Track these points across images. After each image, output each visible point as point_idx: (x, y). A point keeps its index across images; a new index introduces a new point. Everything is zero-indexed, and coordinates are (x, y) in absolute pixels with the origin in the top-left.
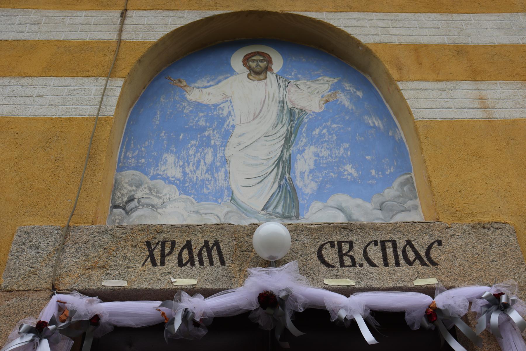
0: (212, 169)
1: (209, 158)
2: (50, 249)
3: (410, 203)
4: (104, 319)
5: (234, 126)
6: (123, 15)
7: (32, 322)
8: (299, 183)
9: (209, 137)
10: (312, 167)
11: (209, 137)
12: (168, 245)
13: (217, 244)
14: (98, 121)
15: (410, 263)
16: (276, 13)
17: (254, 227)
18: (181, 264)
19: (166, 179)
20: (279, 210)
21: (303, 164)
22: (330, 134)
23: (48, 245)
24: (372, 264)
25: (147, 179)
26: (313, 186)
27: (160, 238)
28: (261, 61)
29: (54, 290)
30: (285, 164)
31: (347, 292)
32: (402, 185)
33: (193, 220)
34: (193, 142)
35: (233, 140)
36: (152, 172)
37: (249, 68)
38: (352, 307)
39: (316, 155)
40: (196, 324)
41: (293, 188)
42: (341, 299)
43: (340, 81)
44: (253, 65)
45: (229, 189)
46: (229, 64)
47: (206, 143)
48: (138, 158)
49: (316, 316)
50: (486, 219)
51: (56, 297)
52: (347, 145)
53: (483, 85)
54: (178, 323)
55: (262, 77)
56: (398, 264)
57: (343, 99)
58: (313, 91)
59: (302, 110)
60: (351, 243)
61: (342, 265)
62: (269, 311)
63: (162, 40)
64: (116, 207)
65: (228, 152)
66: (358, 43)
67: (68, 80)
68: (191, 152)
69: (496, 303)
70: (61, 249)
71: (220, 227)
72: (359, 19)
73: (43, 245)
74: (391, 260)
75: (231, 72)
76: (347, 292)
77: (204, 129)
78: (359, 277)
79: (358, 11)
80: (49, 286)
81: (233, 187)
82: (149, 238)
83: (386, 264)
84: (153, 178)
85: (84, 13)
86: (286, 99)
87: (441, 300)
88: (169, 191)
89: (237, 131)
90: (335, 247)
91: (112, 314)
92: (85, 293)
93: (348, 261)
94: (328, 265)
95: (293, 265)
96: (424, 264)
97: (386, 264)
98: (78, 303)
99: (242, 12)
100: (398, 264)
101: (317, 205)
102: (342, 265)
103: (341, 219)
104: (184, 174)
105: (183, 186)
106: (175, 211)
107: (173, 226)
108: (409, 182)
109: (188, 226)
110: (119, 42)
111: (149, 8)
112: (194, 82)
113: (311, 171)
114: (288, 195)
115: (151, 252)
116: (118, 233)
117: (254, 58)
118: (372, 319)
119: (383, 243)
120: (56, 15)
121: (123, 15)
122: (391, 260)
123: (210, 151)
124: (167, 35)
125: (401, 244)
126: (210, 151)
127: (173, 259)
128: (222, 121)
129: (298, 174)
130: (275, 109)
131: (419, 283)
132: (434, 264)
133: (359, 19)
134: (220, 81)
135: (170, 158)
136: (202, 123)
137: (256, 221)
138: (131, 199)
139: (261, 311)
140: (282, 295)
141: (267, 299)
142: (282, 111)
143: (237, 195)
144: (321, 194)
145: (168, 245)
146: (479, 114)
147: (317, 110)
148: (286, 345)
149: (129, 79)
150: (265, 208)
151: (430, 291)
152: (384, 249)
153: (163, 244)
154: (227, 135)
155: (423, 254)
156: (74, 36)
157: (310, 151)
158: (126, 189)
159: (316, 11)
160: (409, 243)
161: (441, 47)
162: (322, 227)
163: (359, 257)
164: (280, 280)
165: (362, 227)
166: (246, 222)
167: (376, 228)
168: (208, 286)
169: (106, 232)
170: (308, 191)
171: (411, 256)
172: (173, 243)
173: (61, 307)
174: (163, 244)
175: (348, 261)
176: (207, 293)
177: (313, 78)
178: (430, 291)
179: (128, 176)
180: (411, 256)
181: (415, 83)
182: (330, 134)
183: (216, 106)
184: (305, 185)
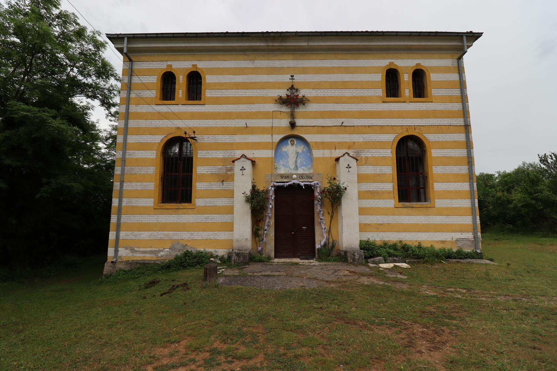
21: (298, 162)
30: (296, 162)
38: (302, 184)
47: (285, 158)
49: (299, 184)
57: (305, 150)
58: (301, 148)
69: (317, 184)
88: (281, 166)
90: (301, 176)
98: (275, 184)
105: (283, 165)
106: (282, 171)
114: (296, 168)
120: (262, 136)
146: (322, 156)
156: (266, 141)
179: (276, 164)
184: (299, 165)
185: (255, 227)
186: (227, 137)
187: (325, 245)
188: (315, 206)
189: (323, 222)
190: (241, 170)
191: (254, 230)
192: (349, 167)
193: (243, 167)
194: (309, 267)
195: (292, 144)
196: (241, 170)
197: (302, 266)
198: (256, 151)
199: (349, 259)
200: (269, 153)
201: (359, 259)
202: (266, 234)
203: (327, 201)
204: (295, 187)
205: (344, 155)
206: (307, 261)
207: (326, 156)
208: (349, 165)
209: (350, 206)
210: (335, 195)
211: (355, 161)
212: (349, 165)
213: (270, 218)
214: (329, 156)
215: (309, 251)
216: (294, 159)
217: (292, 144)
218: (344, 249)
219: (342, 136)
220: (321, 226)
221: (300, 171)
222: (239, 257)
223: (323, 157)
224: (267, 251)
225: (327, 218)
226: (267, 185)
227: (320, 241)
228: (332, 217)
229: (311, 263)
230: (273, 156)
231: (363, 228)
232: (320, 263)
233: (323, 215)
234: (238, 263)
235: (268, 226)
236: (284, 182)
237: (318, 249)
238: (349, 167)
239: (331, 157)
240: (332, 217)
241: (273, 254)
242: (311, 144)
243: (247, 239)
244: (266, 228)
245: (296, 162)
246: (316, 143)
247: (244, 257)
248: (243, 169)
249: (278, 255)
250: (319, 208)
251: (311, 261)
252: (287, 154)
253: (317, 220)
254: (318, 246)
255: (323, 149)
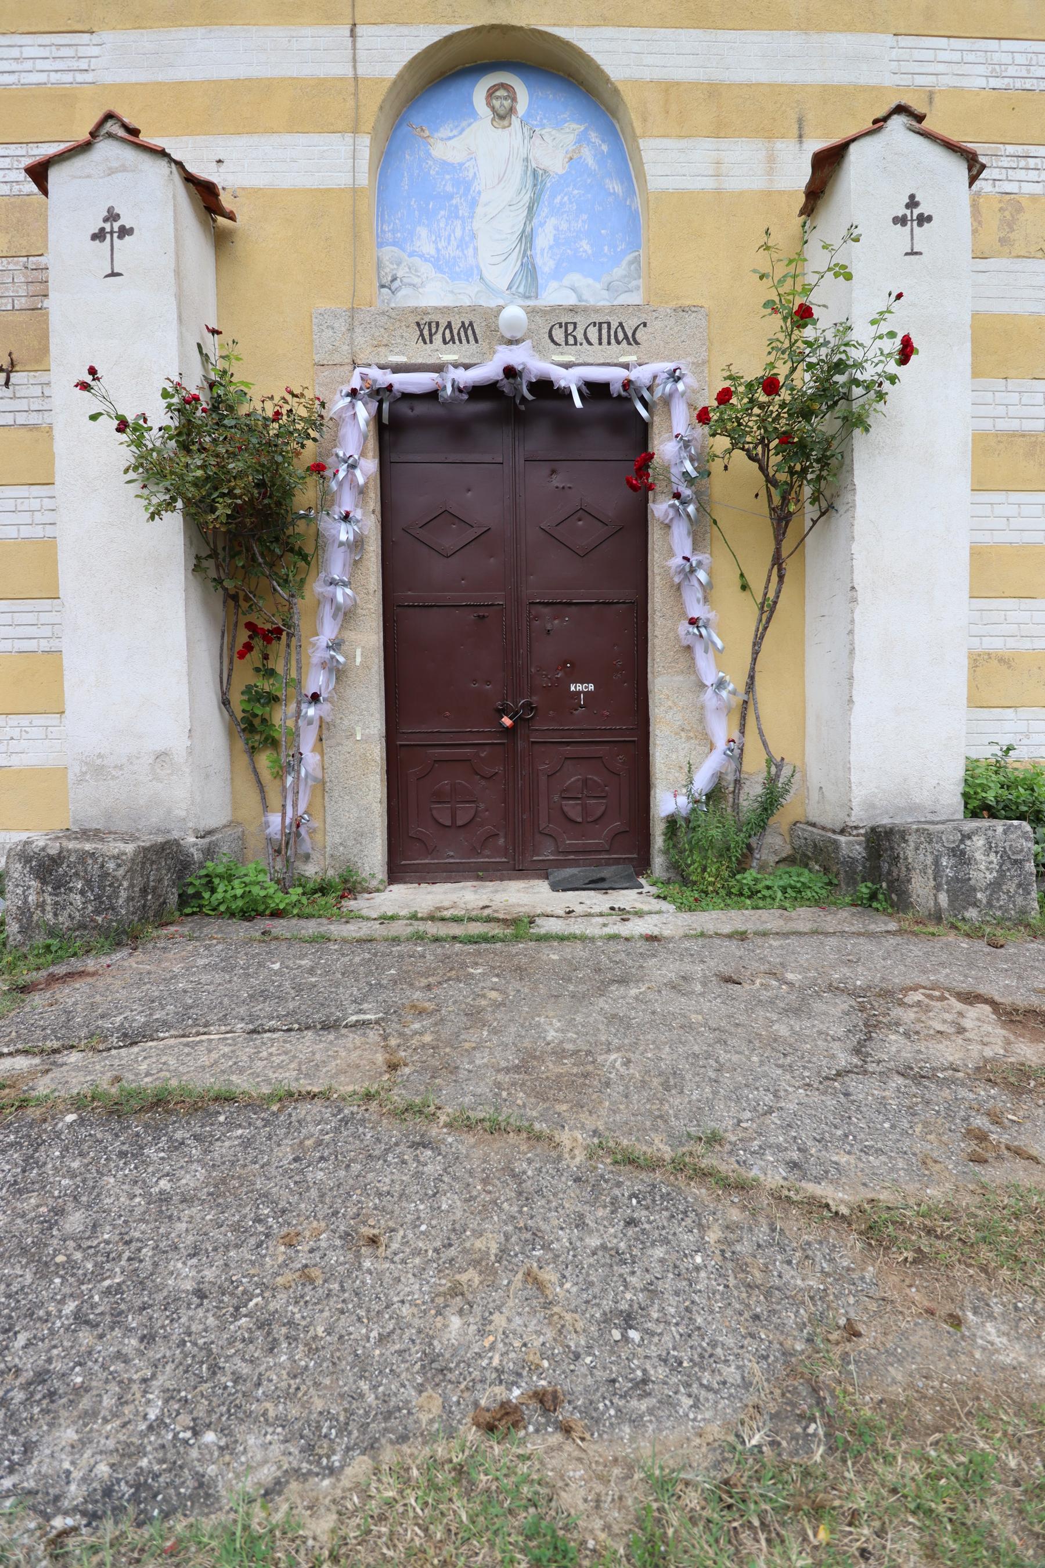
0: (462, 245)
1: (458, 233)
2: (343, 329)
3: (634, 283)
4: (396, 387)
5: (479, 193)
6: (353, 34)
7: (347, 389)
8: (539, 261)
9: (456, 207)
10: (552, 242)
11: (456, 207)
12: (434, 325)
13: (471, 324)
14: (355, 191)
15: (619, 343)
16: (521, 28)
17: (501, 308)
18: (445, 342)
19: (422, 256)
20: (521, 290)
21: (543, 240)
22: (571, 203)
23: (341, 325)
24: (590, 343)
25: (405, 256)
26: (551, 264)
27: (427, 319)
28: (505, 98)
29: (355, 364)
30: (527, 238)
31: (567, 366)
32: (630, 263)
33: (448, 301)
34: (442, 213)
35: (479, 210)
36: (409, 249)
37: (493, 109)
38: (569, 379)
39: (556, 228)
40: (460, 391)
41: (534, 266)
42: (562, 371)
43: (586, 129)
44: (496, 103)
45: (478, 267)
46: (472, 103)
47: (454, 214)
48: (394, 231)
49: (544, 387)
50: (688, 302)
51: (358, 370)
52: (585, 217)
53: (724, 143)
54: (449, 390)
55: (506, 123)
56: (609, 343)
57: (588, 155)
59: (545, 171)
60: (575, 324)
61: (567, 343)
62: (511, 380)
63: (400, 76)
64: (383, 286)
65: (477, 224)
66: (607, 80)
67: (316, 138)
68: (442, 225)
69: (674, 376)
70: (351, 330)
71: (473, 309)
72: (612, 39)
73: (336, 325)
74: (605, 340)
75: (473, 114)
76: (567, 366)
77: (451, 197)
78: (578, 354)
79: (613, 25)
80: (350, 361)
81: (482, 265)
82: (418, 319)
83: (600, 343)
84: (410, 255)
85: (308, 31)
86: (531, 157)
87: (634, 375)
88: (426, 269)
89: (483, 198)
90: (563, 328)
91: (401, 383)
92: (382, 367)
93: (571, 340)
94: (556, 344)
95: (528, 343)
96: (629, 344)
97: (600, 343)
98: (374, 373)
99: (483, 27)
100: (609, 343)
101: (554, 284)
102: (567, 343)
103: (571, 300)
104: (438, 250)
105: (438, 263)
106: (433, 293)
107: (436, 308)
108: (637, 260)
109: (448, 308)
110: (356, 78)
111: (379, 20)
112: (437, 130)
113: (551, 247)
115: (421, 331)
116: (393, 315)
117: (498, 93)
118: (584, 389)
119: (600, 324)
121: (353, 34)
122: (605, 340)
123: (459, 223)
124: (405, 66)
125: (614, 325)
126: (459, 223)
127: (438, 338)
128: (468, 185)
129: (538, 251)
130: (518, 168)
131: (623, 359)
132: (637, 343)
133: (612, 39)
134: (463, 130)
135: (423, 231)
136: (449, 188)
137: (501, 302)
138: (394, 279)
139: (505, 381)
140: (520, 368)
141: (510, 372)
142: (526, 173)
143: (485, 274)
144: (557, 274)
145: (434, 325)
146: (709, 184)
147: (561, 172)
148: (523, 408)
149: (374, 133)
150: (509, 288)
151: (626, 366)
152: (600, 330)
153: (430, 324)
154: (474, 204)
155: (630, 335)
156: (308, 71)
157: (552, 221)
158: (389, 269)
159: (567, 25)
160: (621, 324)
161: (695, 85)
162: (554, 309)
163: (580, 337)
164: (518, 356)
165: (585, 310)
166: (493, 303)
167: (597, 310)
168: (467, 361)
169: (383, 313)
170: (546, 269)
171: (621, 336)
172: (437, 324)
173: (364, 377)
174: (430, 324)
175: (571, 340)
176: (467, 367)
177: (558, 126)
178: (626, 366)
179: (388, 252)
180: (621, 336)
181: (658, 140)
182: (571, 203)
183: (461, 165)
184: (545, 263)
185: (245, 675)
186: (32, 47)
187: (715, 795)
188: (655, 535)
189: (709, 645)
190: (99, 236)
191: (237, 700)
192: (913, 215)
193: (112, 216)
194: (610, 968)
195: (502, 116)
196: (99, 236)
197: (553, 955)
198: (242, 141)
199: (920, 888)
200: (332, 161)
201: (996, 886)
202: (323, 725)
203: (738, 479)
204: (516, 405)
205: (880, 122)
206: (595, 901)
207: (733, 184)
208: (912, 203)
209: (911, 500)
210: (804, 441)
211: (959, 170)
212: (912, 203)
213: (347, 615)
214: (758, 183)
215: (609, 829)
216: (514, 222)
217: (502, 116)
218: (860, 817)
219: (844, 42)
220: (692, 667)
221: (555, 294)
222: (60, 885)
223: (718, 192)
224: (333, 838)
225: (730, 621)
226: (319, 368)
227: (679, 775)
228: (768, 609)
229: (623, 914)
230: (363, 179)
231: (990, 675)
232: (686, 918)
233: (707, 589)
234: (52, 932)
235: (339, 673)
236: (439, 368)
237: (672, 822)
238: (913, 215)
239: (768, 195)
240: (768, 609)
241: (373, 857)
242: (630, 98)
243: (161, 756)
244: (317, 681)
245: (527, 238)
246: (668, 88)
247: (101, 887)
248: (112, 229)
249: (409, 854)
250: (680, 541)
251: (626, 899)
252: (465, 186)
253: (663, 630)
254: (667, 801)
255: (720, 130)
